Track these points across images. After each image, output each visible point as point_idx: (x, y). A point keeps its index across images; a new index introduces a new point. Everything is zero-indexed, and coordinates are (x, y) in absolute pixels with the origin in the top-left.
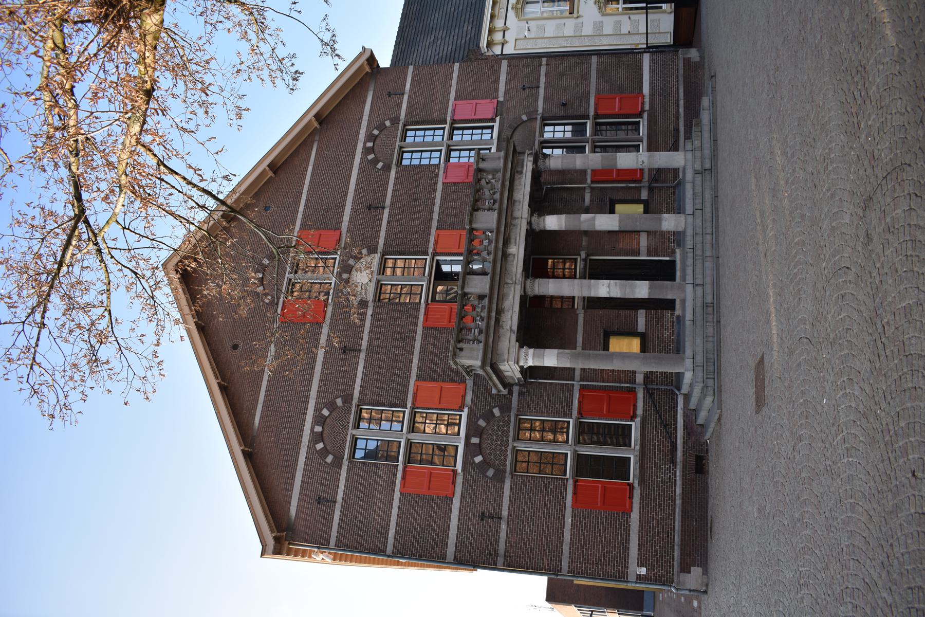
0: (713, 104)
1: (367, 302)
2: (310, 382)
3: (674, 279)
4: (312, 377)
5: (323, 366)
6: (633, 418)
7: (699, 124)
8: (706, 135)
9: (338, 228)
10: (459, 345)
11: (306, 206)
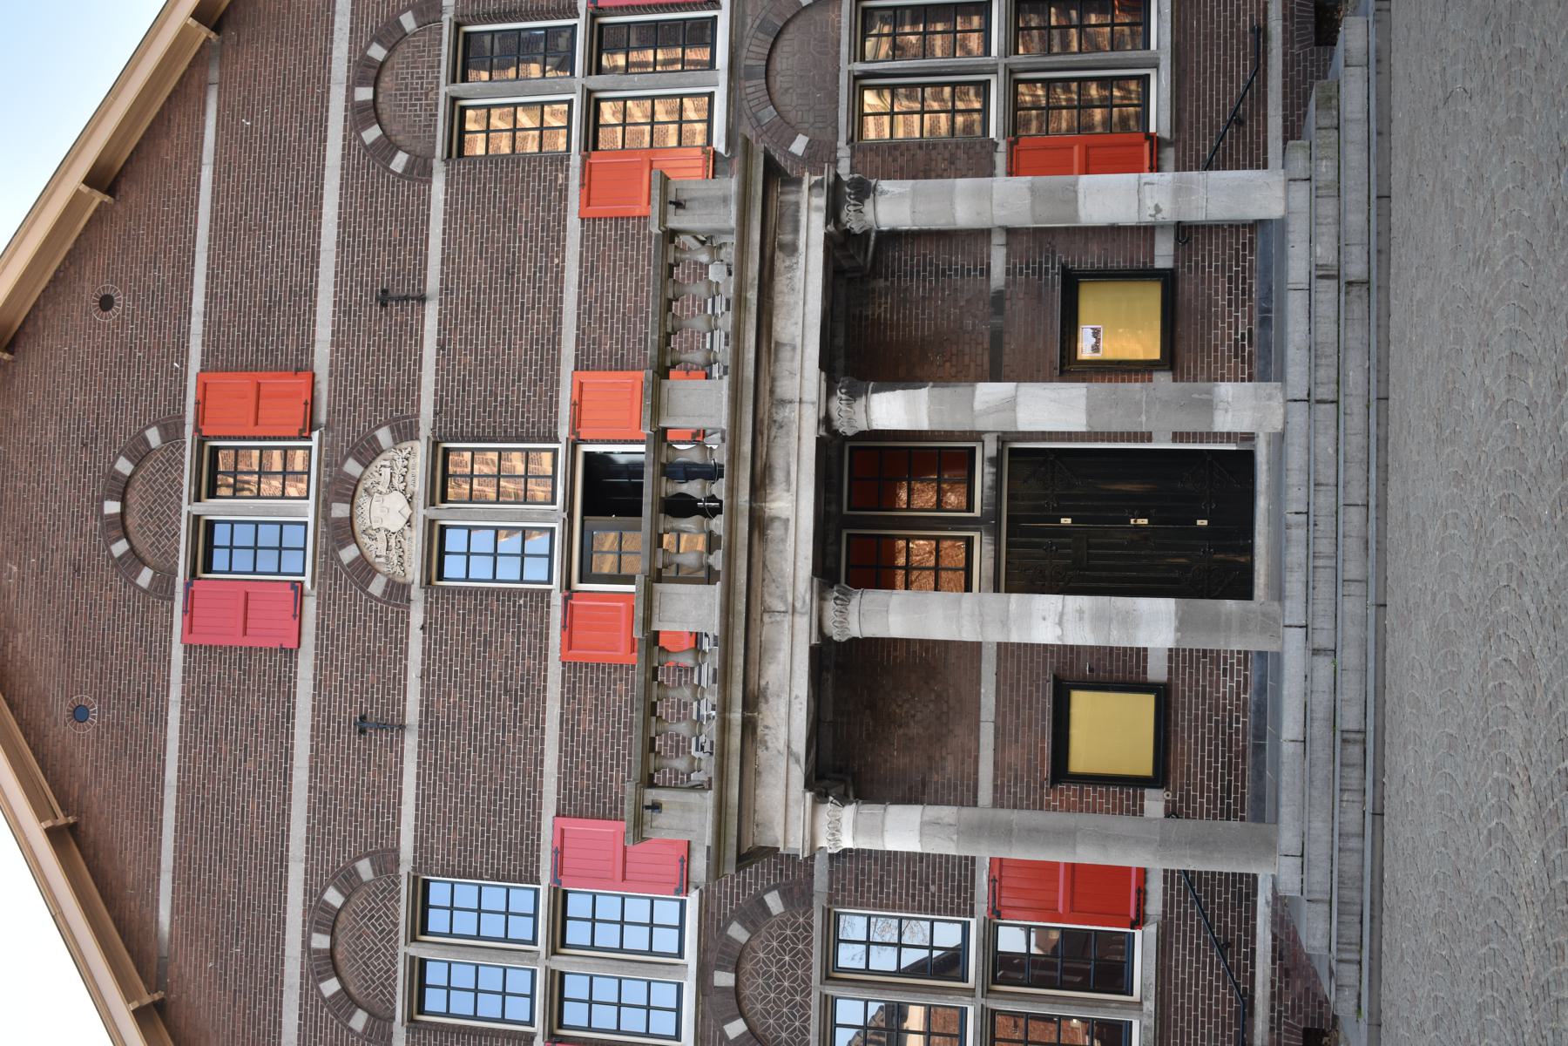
0: (1379, 62)
1: (406, 587)
2: (285, 815)
3: (1247, 594)
4: (287, 799)
5: (313, 769)
6: (1139, 922)
7: (1331, 101)
8: (1355, 133)
9: (304, 368)
10: (651, 795)
11: (210, 296)
